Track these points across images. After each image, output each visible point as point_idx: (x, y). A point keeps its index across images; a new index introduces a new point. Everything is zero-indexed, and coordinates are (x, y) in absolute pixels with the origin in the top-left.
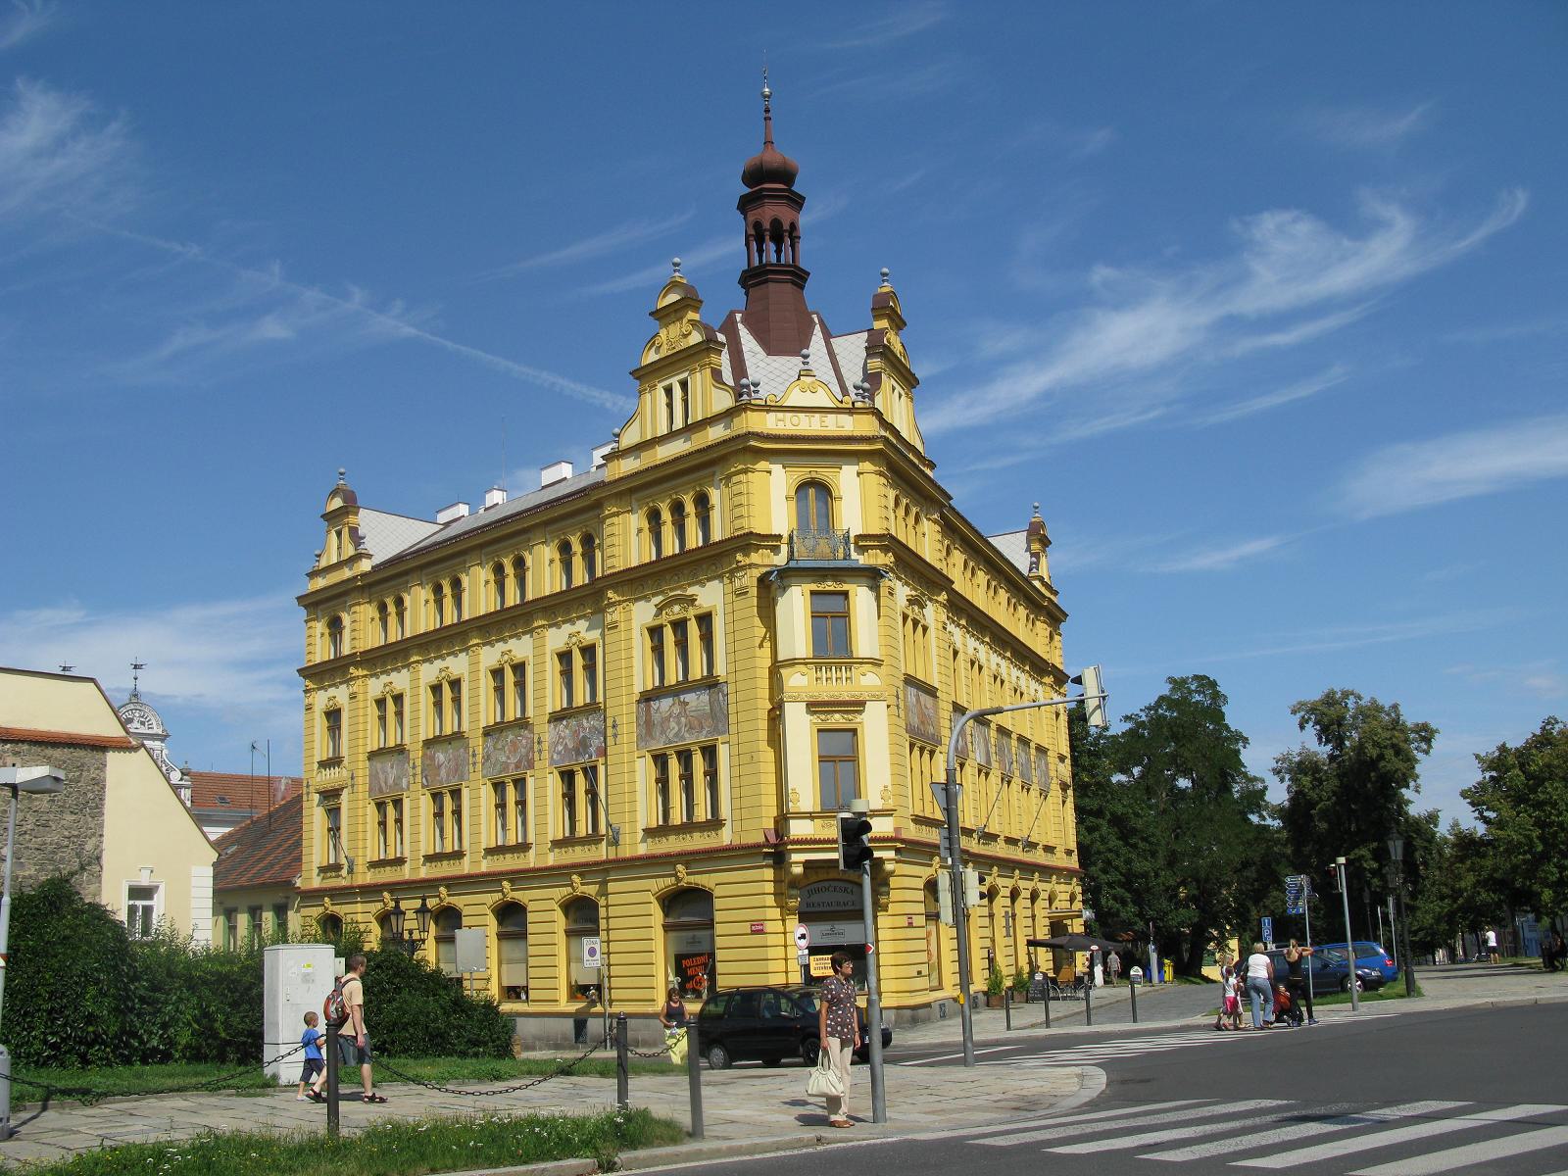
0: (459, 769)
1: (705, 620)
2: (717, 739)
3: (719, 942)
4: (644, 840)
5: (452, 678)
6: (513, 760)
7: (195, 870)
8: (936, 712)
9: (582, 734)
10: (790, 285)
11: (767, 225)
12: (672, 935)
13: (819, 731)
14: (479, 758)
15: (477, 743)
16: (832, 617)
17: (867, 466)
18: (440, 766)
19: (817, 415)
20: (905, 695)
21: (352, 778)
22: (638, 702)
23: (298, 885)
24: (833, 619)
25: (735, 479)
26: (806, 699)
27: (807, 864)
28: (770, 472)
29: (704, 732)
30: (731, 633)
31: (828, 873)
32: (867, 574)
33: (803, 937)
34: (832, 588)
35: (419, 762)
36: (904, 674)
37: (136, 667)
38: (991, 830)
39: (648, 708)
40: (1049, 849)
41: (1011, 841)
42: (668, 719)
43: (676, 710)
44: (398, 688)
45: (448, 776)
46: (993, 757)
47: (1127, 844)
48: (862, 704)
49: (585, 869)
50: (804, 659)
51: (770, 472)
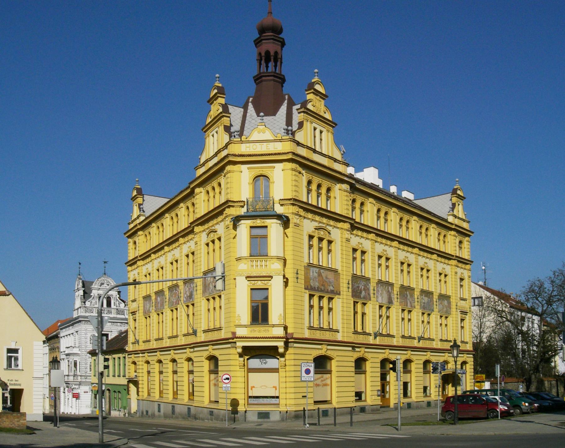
3: (379, 370)
5: (388, 257)
7: (35, 343)
13: (251, 289)
15: (167, 293)
21: (139, 307)
23: (126, 349)
24: (261, 239)
35: (154, 302)
37: (105, 262)
48: (272, 277)
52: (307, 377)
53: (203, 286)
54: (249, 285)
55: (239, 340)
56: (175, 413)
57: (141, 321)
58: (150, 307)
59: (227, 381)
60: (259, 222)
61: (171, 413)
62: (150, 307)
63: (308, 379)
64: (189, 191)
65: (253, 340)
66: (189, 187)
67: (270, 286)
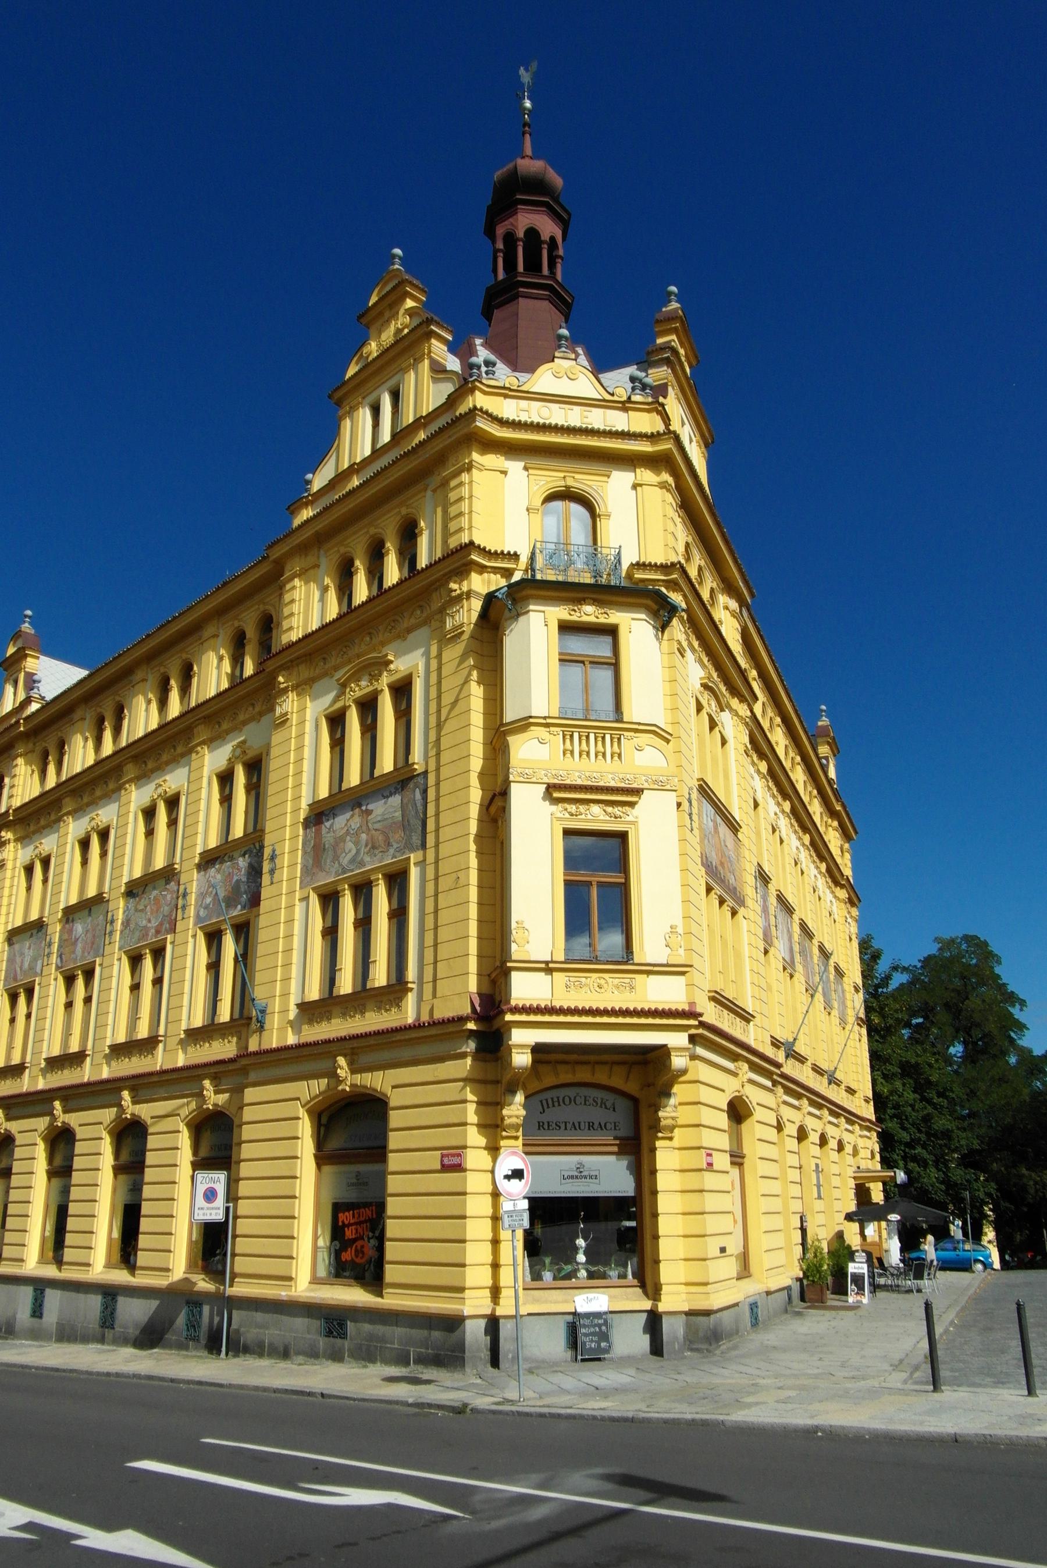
0: (98, 943)
1: (402, 691)
3: (394, 1184)
6: (154, 923)
8: (738, 855)
9: (235, 878)
10: (546, 304)
11: (521, 234)
15: (119, 908)
16: (591, 662)
17: (646, 475)
18: (77, 940)
19: (577, 408)
20: (699, 815)
26: (546, 780)
27: (539, 1050)
28: (504, 473)
29: (392, 851)
31: (574, 1073)
32: (649, 602)
33: (517, 1174)
34: (592, 619)
36: (698, 780)
38: (800, 1048)
39: (318, 834)
40: (851, 1091)
41: (817, 1070)
42: (342, 839)
45: (83, 952)
46: (798, 958)
47: (923, 1099)
48: (638, 792)
49: (217, 1070)
50: (545, 718)
51: (504, 473)
52: (208, 1209)
54: (560, 815)
55: (523, 1018)
58: (35, 960)
60: (589, 614)
63: (211, 1214)
64: (265, 568)
65: (576, 1019)
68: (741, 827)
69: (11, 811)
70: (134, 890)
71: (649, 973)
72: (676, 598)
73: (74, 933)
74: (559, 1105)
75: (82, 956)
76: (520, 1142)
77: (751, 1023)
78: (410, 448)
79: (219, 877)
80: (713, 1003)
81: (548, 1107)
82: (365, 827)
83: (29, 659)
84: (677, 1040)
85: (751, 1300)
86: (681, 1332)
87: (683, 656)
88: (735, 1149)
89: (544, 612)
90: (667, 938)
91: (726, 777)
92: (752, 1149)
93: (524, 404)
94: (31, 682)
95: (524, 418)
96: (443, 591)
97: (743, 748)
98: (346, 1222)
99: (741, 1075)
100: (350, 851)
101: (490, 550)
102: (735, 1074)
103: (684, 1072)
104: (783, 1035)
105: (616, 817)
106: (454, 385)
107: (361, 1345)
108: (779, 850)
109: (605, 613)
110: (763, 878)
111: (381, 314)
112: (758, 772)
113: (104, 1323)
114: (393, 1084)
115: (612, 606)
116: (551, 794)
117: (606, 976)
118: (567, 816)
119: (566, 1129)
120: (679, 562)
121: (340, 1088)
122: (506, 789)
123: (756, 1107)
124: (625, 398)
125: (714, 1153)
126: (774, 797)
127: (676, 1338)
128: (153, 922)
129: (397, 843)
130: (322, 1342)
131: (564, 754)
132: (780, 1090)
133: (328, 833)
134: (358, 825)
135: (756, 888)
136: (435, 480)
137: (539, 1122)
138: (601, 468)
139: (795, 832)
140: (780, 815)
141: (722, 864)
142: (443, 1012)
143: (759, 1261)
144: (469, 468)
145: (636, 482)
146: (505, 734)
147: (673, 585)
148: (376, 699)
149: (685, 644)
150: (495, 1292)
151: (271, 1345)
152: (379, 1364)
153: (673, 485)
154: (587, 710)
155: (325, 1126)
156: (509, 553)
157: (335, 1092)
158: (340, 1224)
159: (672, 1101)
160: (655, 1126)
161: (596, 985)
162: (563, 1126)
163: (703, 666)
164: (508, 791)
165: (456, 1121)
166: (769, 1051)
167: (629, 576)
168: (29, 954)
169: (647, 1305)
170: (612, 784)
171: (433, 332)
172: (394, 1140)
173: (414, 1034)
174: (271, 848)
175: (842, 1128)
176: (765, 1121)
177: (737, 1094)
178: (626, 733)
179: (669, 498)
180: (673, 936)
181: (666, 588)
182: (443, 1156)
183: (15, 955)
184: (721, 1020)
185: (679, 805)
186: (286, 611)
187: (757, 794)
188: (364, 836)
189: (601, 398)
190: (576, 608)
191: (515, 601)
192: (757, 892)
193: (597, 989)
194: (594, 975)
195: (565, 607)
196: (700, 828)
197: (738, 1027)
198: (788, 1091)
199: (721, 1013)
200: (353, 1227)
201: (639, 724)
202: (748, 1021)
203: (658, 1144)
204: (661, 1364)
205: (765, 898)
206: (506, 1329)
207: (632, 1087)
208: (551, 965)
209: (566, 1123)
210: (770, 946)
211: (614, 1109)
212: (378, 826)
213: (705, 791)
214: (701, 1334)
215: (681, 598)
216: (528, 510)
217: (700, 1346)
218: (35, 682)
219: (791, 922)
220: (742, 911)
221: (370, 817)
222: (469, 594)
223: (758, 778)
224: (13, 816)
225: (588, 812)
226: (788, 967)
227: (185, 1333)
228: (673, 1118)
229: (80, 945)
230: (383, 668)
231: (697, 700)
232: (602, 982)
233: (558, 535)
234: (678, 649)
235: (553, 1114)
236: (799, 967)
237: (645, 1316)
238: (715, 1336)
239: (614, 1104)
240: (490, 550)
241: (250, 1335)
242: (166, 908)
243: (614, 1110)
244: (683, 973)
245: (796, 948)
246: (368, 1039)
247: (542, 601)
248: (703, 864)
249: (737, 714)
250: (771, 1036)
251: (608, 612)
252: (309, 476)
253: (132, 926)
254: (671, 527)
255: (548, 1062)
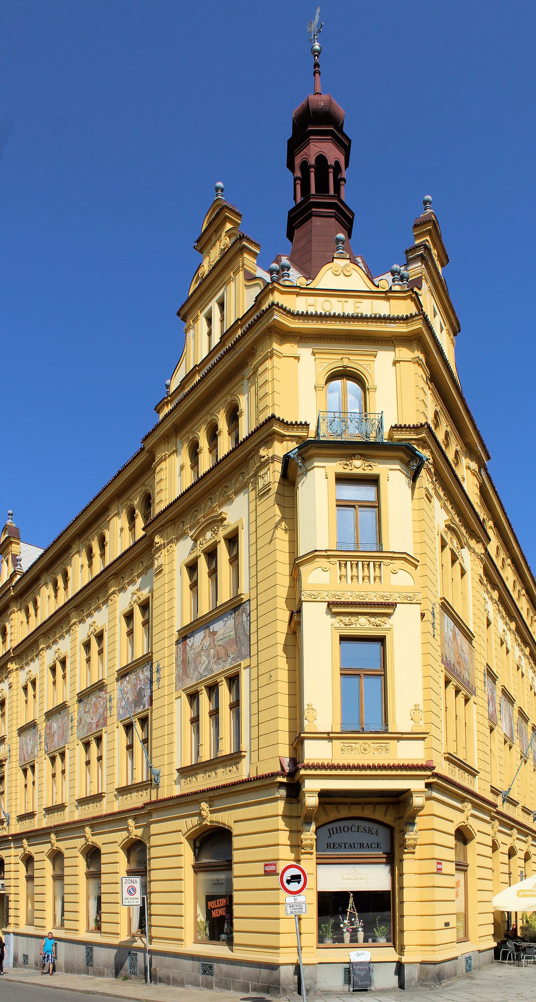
2: (240, 665)
3: (237, 883)
4: (177, 782)
6: (95, 721)
8: (472, 658)
9: (139, 687)
12: (202, 876)
13: (343, 639)
14: (75, 723)
15: (74, 708)
17: (404, 353)
19: (351, 300)
20: (442, 625)
21: (9, 751)
22: (177, 643)
25: (261, 369)
26: (327, 599)
27: (323, 794)
29: (230, 660)
30: (255, 544)
32: (401, 454)
34: (360, 471)
35: (43, 733)
36: (441, 599)
38: (513, 795)
42: (199, 654)
43: (207, 643)
44: (33, 675)
45: (58, 741)
46: (516, 735)
48: (393, 605)
50: (326, 551)
51: (297, 358)
52: (131, 899)
53: (177, 666)
54: (337, 625)
56: (94, 963)
57: (14, 777)
58: (33, 747)
59: (294, 886)
61: (85, 963)
62: (33, 747)
63: (133, 902)
64: (143, 457)
66: (142, 449)
67: (389, 629)
68: (474, 637)
69: (11, 650)
70: (82, 697)
71: (399, 739)
72: (425, 453)
73: (53, 729)
74: (341, 832)
75: (58, 744)
76: (314, 856)
77: (477, 777)
78: (230, 345)
79: (129, 686)
80: (447, 762)
81: (334, 833)
82: (212, 645)
83: (13, 545)
84: (417, 785)
85: (467, 955)
86: (416, 975)
87: (430, 502)
88: (462, 860)
89: (325, 467)
90: (412, 714)
91: (464, 598)
92: (472, 860)
93: (311, 299)
94: (16, 561)
95: (311, 310)
96: (256, 458)
97: (478, 578)
98: (213, 907)
99: (466, 812)
100: (204, 662)
101: (287, 422)
102: (462, 811)
103: (422, 808)
104: (502, 787)
105: (377, 626)
106: (261, 288)
107: (222, 979)
108: (505, 658)
109: (370, 466)
110: (491, 675)
111: (210, 239)
112: (491, 598)
113: (88, 963)
114: (235, 820)
115: (375, 460)
116: (331, 610)
117: (369, 742)
118: (342, 625)
119: (345, 848)
120: (427, 423)
121: (204, 823)
122: (300, 608)
123: (477, 833)
124: (387, 289)
125: (443, 862)
126: (503, 618)
127: (413, 979)
128: (94, 719)
129: (233, 654)
130: (201, 977)
131: (340, 578)
132: (496, 823)
133: (190, 650)
134: (209, 644)
135: (485, 682)
136: (248, 372)
137: (327, 844)
138: (368, 348)
139: (519, 645)
140: (508, 632)
141: (459, 663)
142: (264, 770)
143: (474, 931)
144: (271, 355)
145: (395, 359)
146: (299, 565)
147: (423, 443)
148: (216, 549)
149: (432, 492)
150: (299, 949)
151: (173, 978)
152: (232, 991)
153: (424, 361)
154: (357, 544)
155: (198, 848)
156: (301, 423)
157: (201, 826)
158: (209, 908)
159: (416, 828)
160: (403, 845)
161: (362, 748)
162: (343, 846)
163: (448, 512)
164: (301, 610)
165: (273, 843)
166: (490, 797)
167: (390, 438)
168: (30, 743)
169: (396, 957)
170: (375, 600)
171: (244, 247)
172: (237, 856)
173: (246, 786)
174: (157, 663)
175: (529, 843)
176: (483, 842)
177: (463, 824)
178: (384, 561)
179: (420, 371)
180: (416, 712)
181: (418, 446)
182: (266, 865)
183: (23, 745)
184: (453, 773)
185: (423, 615)
186: (157, 489)
187: (490, 614)
188: (212, 651)
189: (369, 290)
190: (348, 463)
191: (304, 460)
192: (485, 685)
193: (363, 751)
194: (361, 742)
195: (340, 462)
196: (442, 635)
197: (467, 780)
198: (502, 824)
199: (453, 769)
200: (217, 910)
201: (394, 553)
202: (474, 776)
203: (405, 856)
204: (402, 993)
205: (493, 691)
206: (304, 972)
207: (388, 819)
208: (331, 735)
209: (345, 844)
210: (495, 725)
211: (377, 833)
212: (220, 643)
213: (446, 607)
214: (430, 976)
215: (428, 454)
216: (315, 388)
217: (429, 983)
218: (17, 560)
219: (512, 710)
220: (473, 699)
221: (215, 637)
222: (273, 459)
223: (491, 603)
224: (13, 654)
225: (357, 622)
226: (508, 741)
227: (129, 970)
228: (415, 839)
229: (56, 737)
230: (219, 524)
231: (442, 537)
232: (366, 746)
233: (339, 408)
234: (426, 495)
235: (337, 838)
236: (516, 741)
237: (395, 965)
238: (439, 978)
239: (377, 831)
240: (287, 422)
241: (161, 973)
242: (101, 710)
243: (377, 835)
244: (423, 739)
245: (515, 727)
246: (219, 790)
247: (324, 459)
248: (442, 662)
249: (474, 552)
250: (491, 786)
251: (372, 465)
252: (168, 382)
253: (83, 722)
254: (422, 396)
255: (333, 804)
